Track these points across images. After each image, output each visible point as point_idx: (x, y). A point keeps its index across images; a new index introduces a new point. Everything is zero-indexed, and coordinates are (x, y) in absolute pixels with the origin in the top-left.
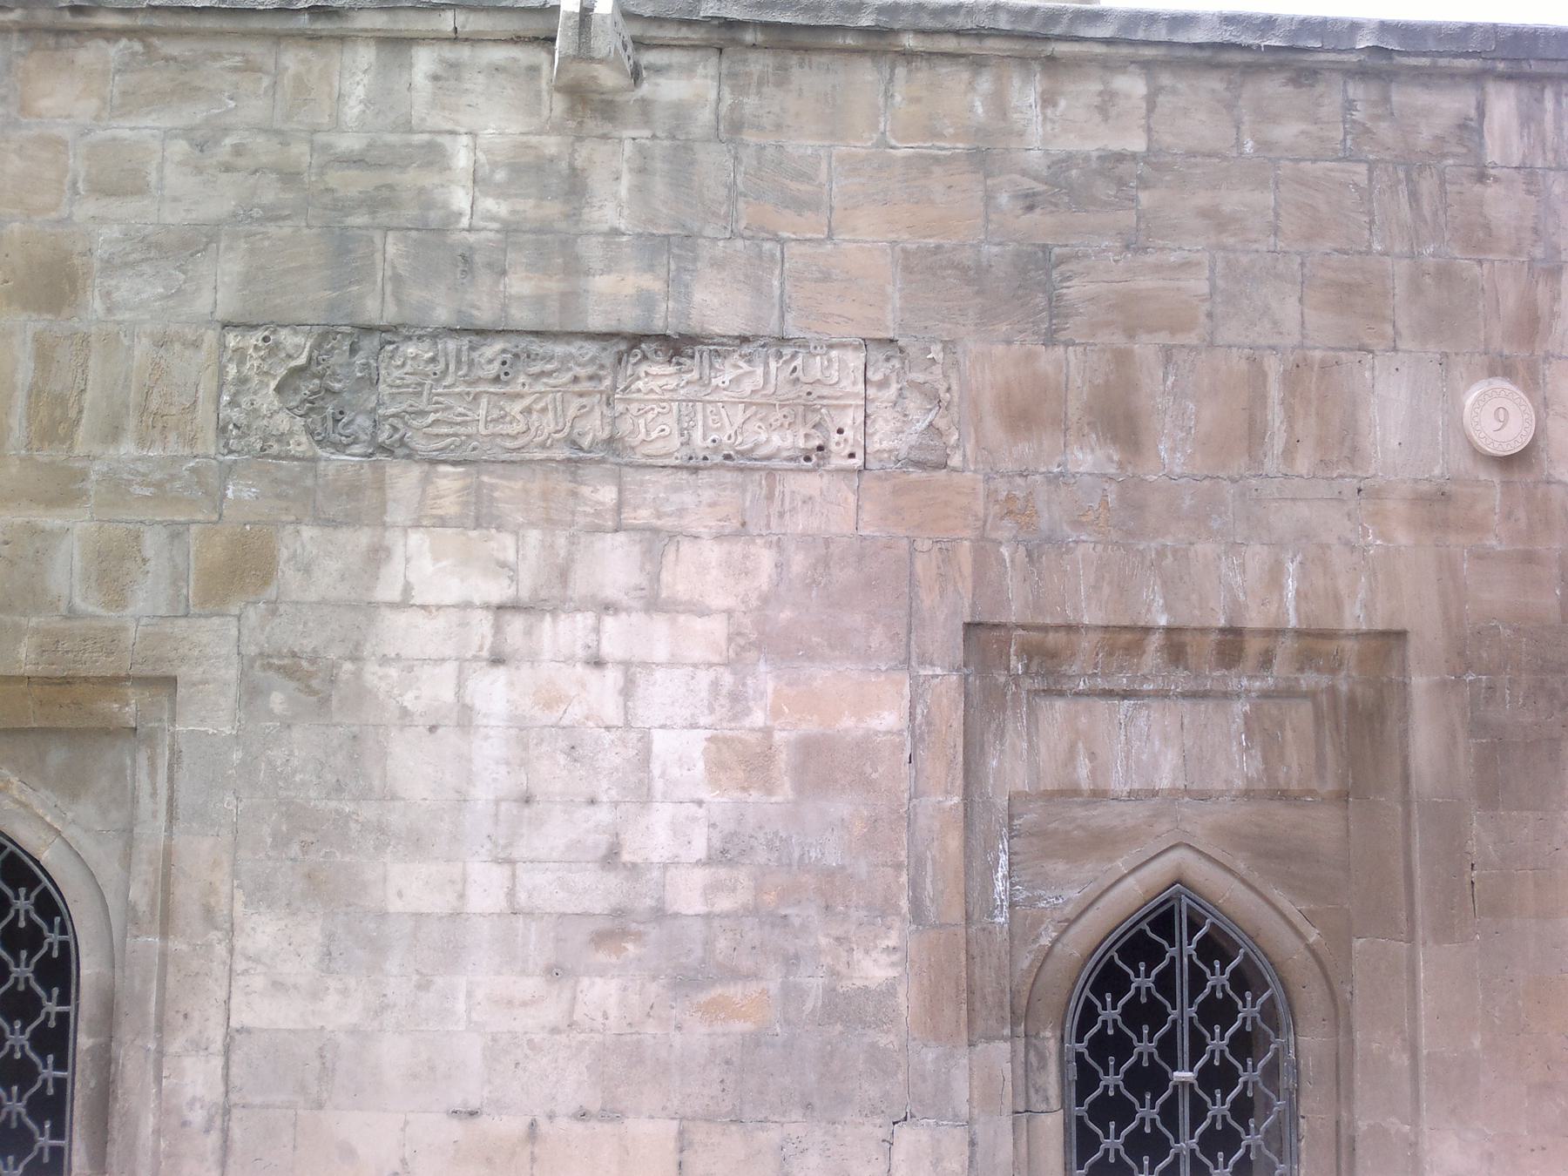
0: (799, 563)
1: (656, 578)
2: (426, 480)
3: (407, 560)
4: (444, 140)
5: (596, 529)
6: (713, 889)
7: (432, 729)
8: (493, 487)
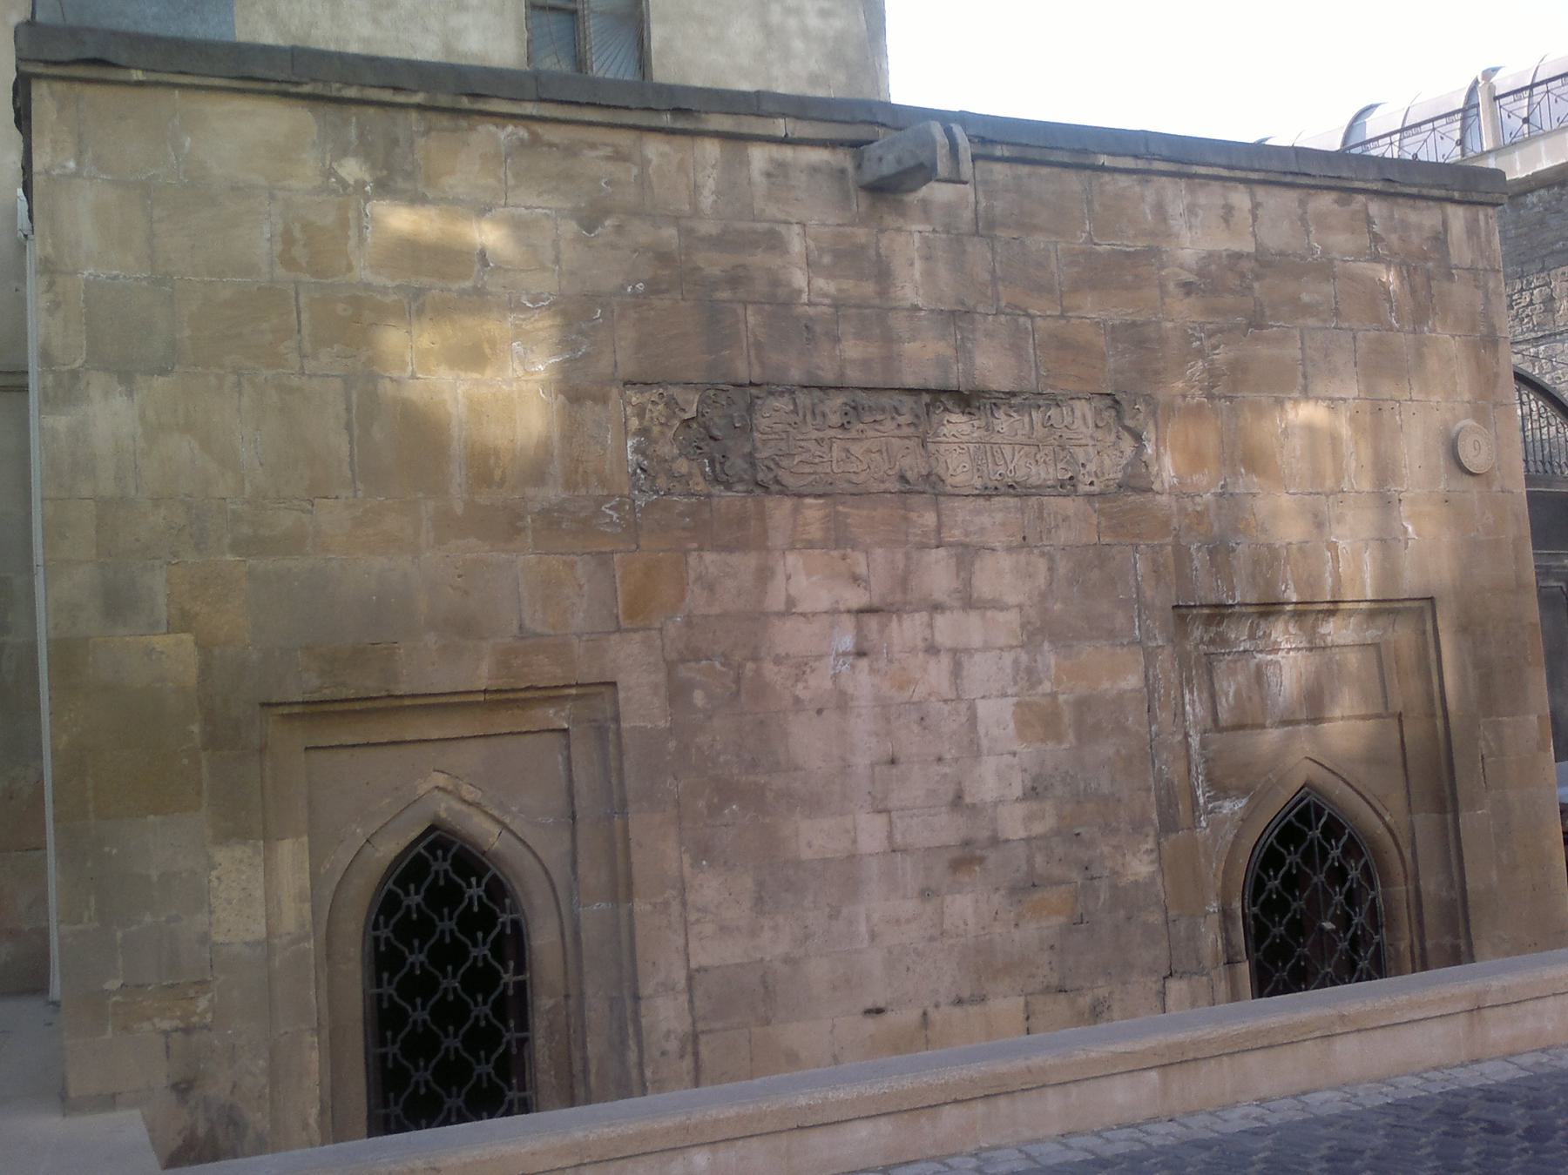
0: (1063, 567)
1: (968, 583)
2: (796, 511)
3: (789, 578)
4: (781, 228)
5: (923, 546)
6: (1030, 818)
7: (820, 712)
8: (847, 515)
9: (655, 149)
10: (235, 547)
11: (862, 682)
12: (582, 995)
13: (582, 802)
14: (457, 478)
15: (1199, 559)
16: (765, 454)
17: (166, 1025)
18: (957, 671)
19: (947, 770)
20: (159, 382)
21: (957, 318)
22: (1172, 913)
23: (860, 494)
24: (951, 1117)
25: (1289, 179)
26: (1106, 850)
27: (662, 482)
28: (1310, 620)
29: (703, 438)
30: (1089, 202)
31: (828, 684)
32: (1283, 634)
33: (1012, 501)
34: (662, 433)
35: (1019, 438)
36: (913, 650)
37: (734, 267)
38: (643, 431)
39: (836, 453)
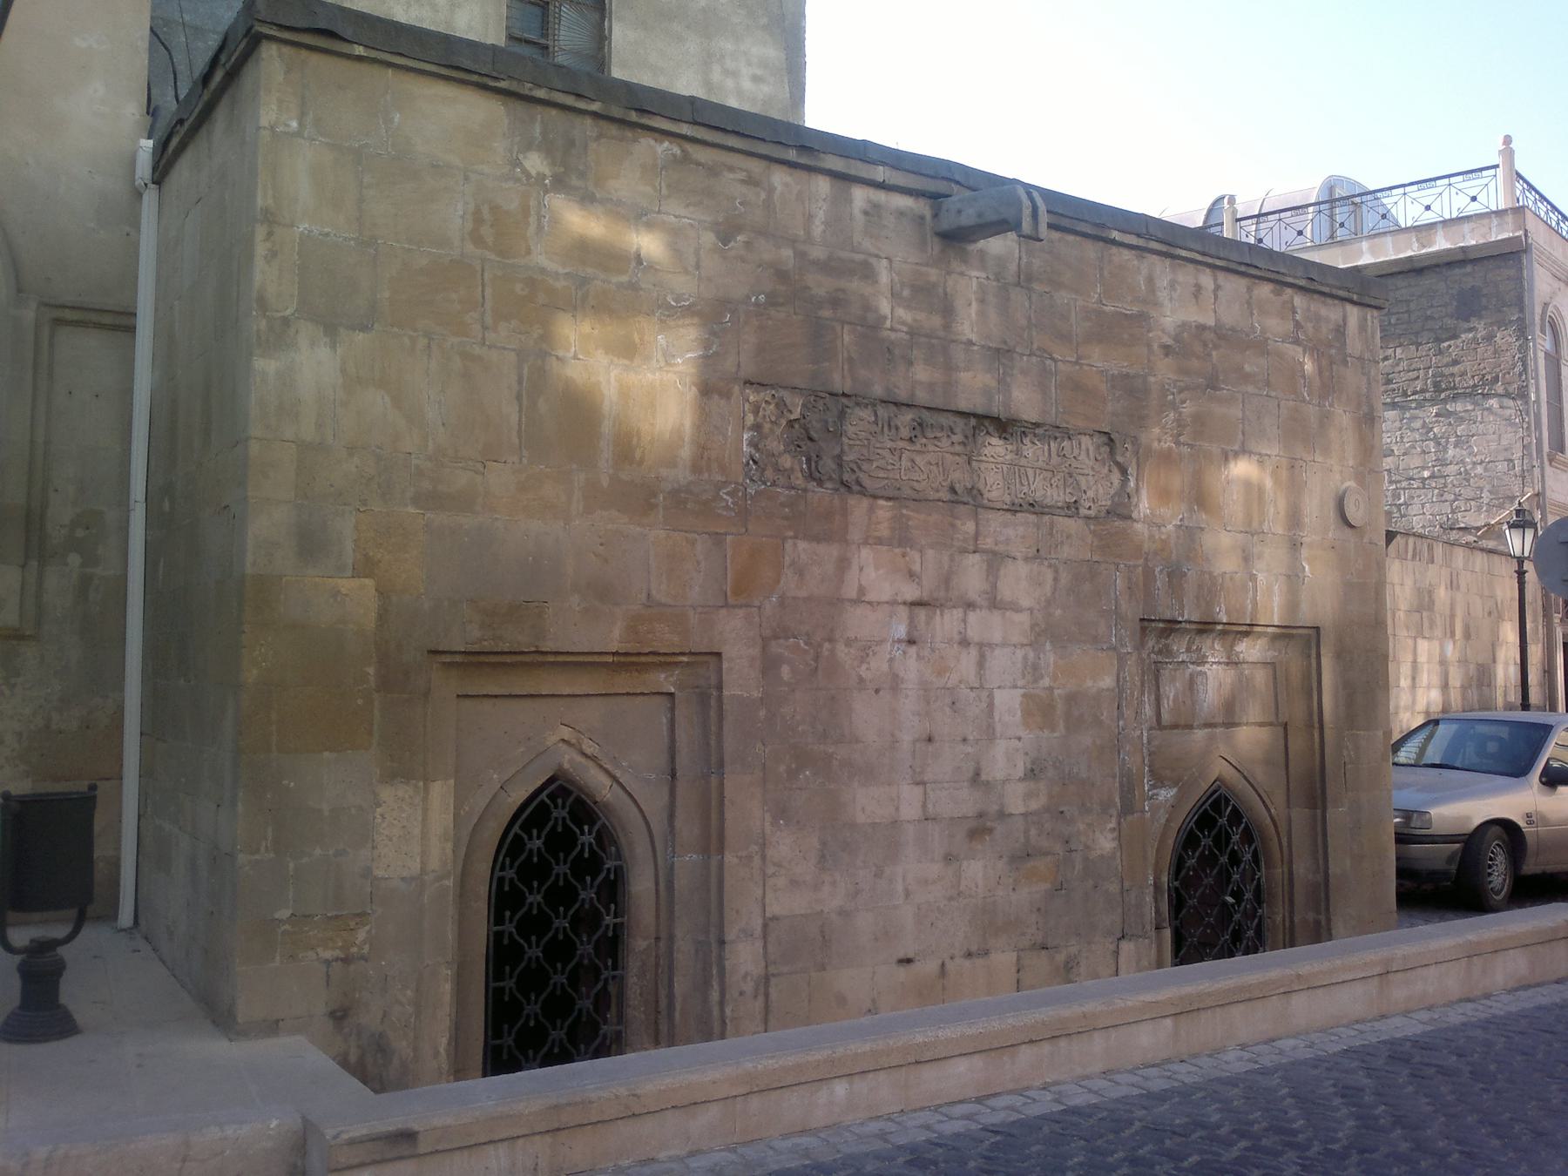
0: (1065, 578)
1: (994, 586)
2: (871, 510)
3: (861, 569)
4: (873, 260)
5: (964, 551)
6: (1028, 796)
7: (877, 691)
8: (909, 518)
9: (780, 178)
10: (416, 501)
11: (912, 667)
12: (671, 938)
13: (683, 760)
14: (606, 454)
15: (1161, 581)
16: (851, 457)
17: (328, 954)
18: (981, 664)
19: (970, 750)
20: (360, 337)
21: (1000, 355)
22: (1127, 885)
23: (919, 500)
24: (1026, 1054)
25: (1243, 269)
26: (1082, 827)
27: (769, 474)
28: (1231, 638)
29: (802, 437)
30: (1101, 269)
31: (885, 667)
32: (1214, 651)
33: (1032, 518)
34: (771, 430)
35: (1040, 464)
36: (950, 641)
37: (838, 290)
38: (757, 427)
39: (905, 463)
